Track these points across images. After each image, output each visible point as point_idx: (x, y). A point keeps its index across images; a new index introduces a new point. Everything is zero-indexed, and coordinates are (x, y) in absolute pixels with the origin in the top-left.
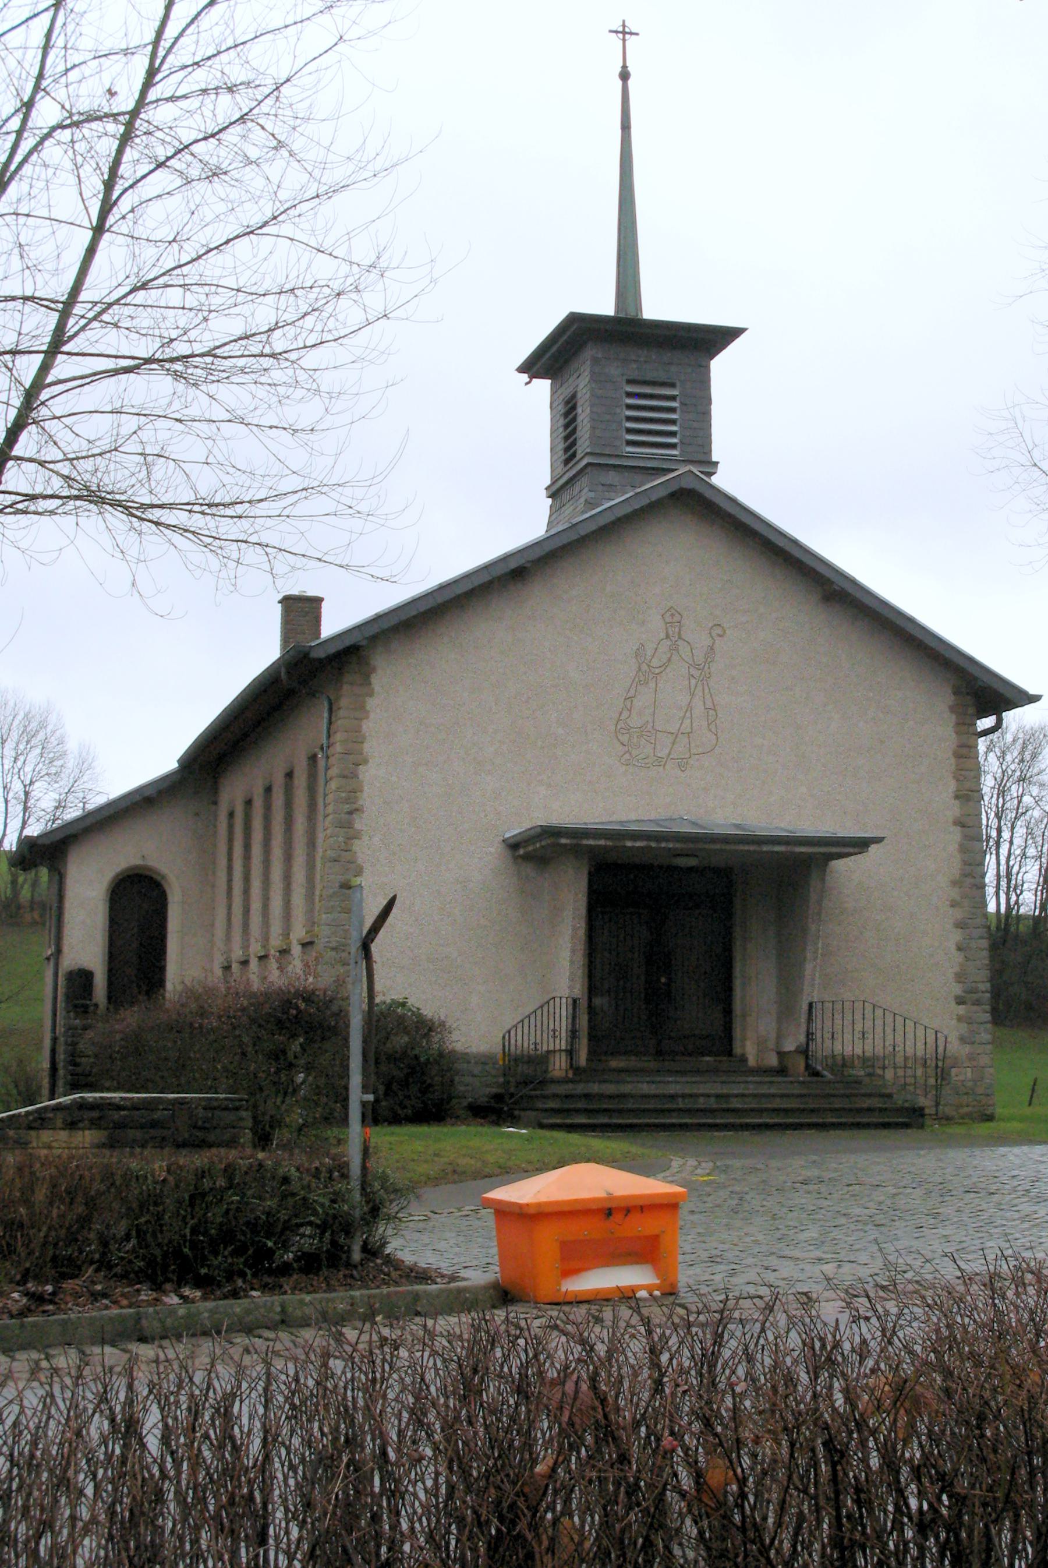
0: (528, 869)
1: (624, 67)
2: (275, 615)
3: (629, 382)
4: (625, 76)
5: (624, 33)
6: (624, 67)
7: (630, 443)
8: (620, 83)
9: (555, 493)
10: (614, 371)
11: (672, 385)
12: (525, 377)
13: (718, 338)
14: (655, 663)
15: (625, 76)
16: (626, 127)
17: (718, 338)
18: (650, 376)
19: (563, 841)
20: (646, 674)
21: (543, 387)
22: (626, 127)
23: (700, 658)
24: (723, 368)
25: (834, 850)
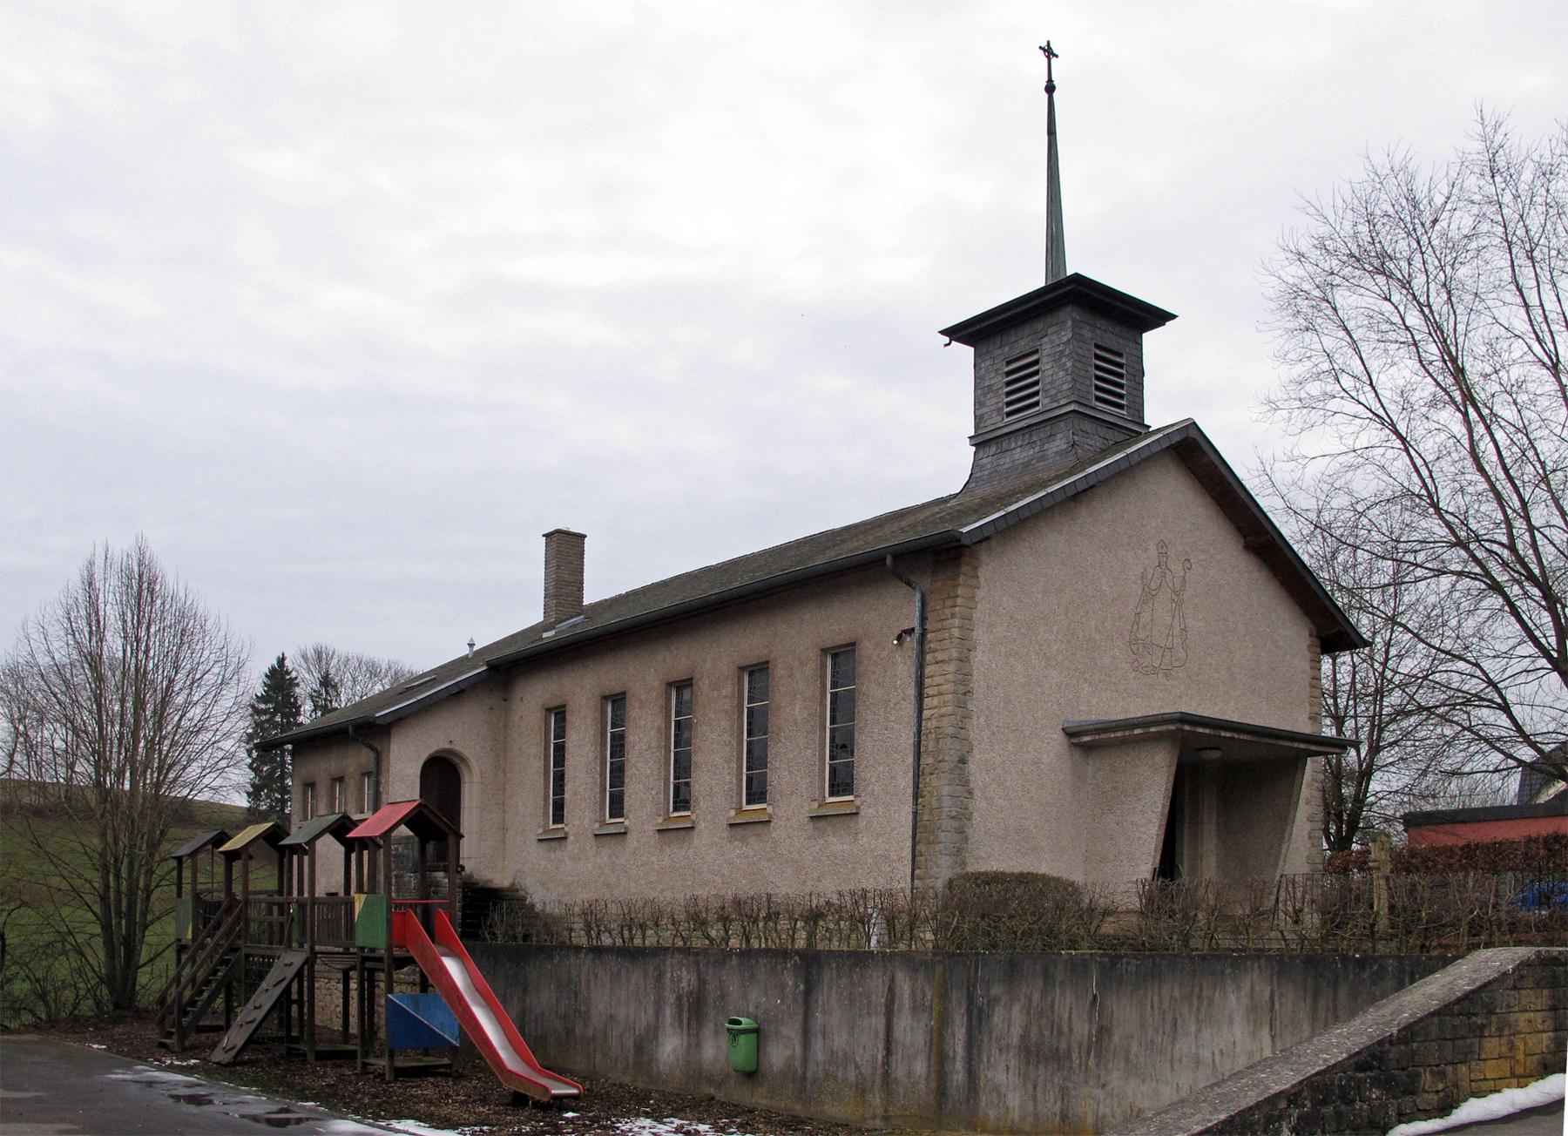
0: (1077, 755)
1: (1050, 80)
2: (538, 550)
3: (1097, 346)
4: (1050, 88)
5: (1049, 52)
6: (1050, 80)
7: (1098, 399)
8: (1046, 96)
9: (980, 442)
10: (1087, 333)
11: (1120, 355)
12: (947, 340)
13: (1159, 317)
14: (1153, 586)
15: (1050, 88)
16: (1051, 132)
17: (1159, 317)
18: (1016, 353)
19: (1137, 732)
20: (1148, 596)
21: (965, 353)
22: (1051, 132)
23: (1178, 586)
24: (1153, 342)
25: (1313, 748)
